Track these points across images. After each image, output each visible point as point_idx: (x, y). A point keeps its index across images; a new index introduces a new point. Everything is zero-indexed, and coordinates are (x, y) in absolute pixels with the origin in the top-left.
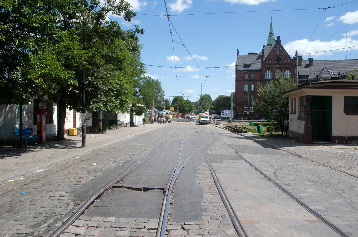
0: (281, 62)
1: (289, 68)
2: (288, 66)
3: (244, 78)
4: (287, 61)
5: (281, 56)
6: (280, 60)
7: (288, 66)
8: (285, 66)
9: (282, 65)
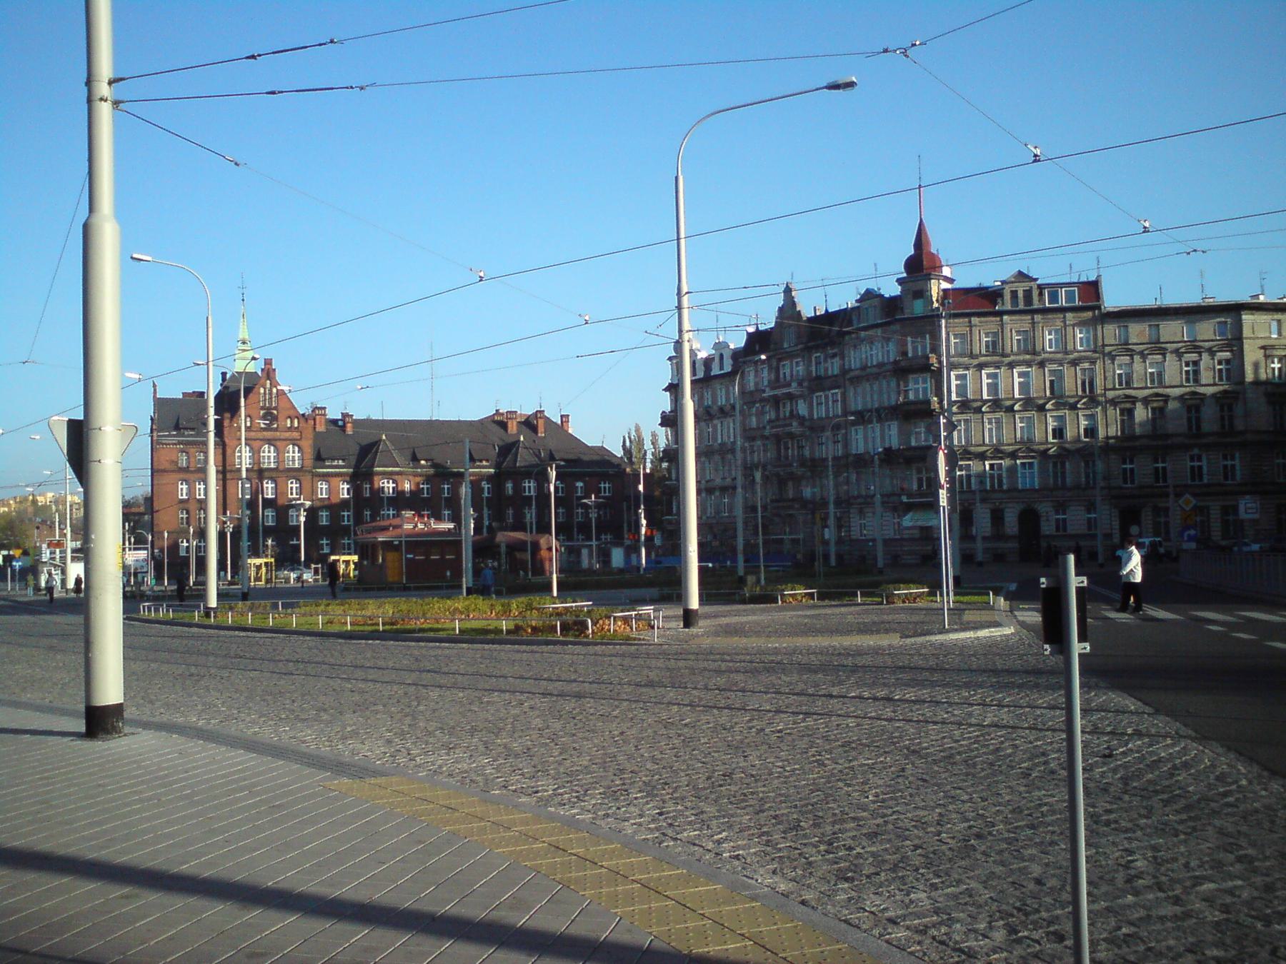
0: (275, 426)
1: (295, 440)
2: (296, 435)
3: (177, 463)
4: (292, 422)
5: (275, 408)
6: (275, 418)
7: (296, 435)
8: (287, 435)
9: (278, 433)
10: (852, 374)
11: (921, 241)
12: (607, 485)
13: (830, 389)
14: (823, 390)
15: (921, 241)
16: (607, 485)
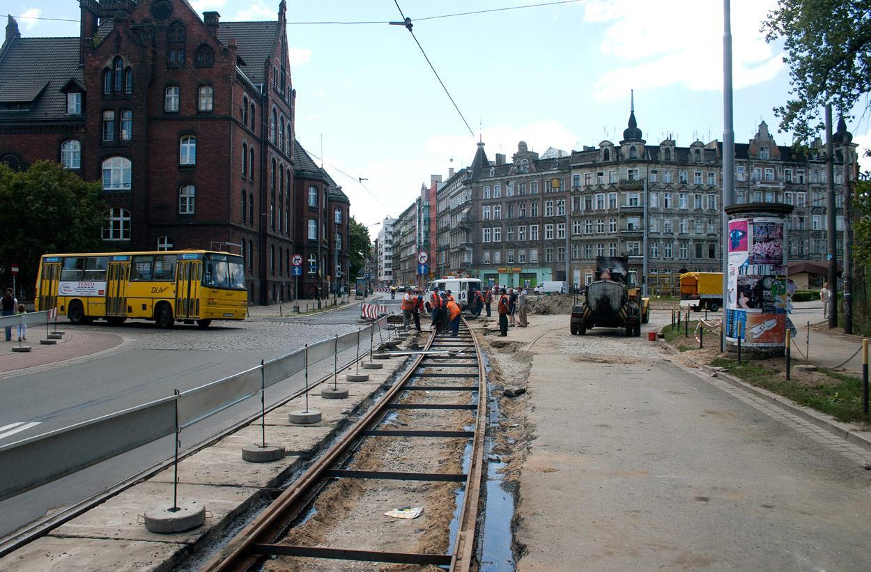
10: (814, 185)
11: (632, 121)
12: (122, 219)
13: (797, 191)
14: (793, 191)
15: (632, 121)
16: (122, 219)
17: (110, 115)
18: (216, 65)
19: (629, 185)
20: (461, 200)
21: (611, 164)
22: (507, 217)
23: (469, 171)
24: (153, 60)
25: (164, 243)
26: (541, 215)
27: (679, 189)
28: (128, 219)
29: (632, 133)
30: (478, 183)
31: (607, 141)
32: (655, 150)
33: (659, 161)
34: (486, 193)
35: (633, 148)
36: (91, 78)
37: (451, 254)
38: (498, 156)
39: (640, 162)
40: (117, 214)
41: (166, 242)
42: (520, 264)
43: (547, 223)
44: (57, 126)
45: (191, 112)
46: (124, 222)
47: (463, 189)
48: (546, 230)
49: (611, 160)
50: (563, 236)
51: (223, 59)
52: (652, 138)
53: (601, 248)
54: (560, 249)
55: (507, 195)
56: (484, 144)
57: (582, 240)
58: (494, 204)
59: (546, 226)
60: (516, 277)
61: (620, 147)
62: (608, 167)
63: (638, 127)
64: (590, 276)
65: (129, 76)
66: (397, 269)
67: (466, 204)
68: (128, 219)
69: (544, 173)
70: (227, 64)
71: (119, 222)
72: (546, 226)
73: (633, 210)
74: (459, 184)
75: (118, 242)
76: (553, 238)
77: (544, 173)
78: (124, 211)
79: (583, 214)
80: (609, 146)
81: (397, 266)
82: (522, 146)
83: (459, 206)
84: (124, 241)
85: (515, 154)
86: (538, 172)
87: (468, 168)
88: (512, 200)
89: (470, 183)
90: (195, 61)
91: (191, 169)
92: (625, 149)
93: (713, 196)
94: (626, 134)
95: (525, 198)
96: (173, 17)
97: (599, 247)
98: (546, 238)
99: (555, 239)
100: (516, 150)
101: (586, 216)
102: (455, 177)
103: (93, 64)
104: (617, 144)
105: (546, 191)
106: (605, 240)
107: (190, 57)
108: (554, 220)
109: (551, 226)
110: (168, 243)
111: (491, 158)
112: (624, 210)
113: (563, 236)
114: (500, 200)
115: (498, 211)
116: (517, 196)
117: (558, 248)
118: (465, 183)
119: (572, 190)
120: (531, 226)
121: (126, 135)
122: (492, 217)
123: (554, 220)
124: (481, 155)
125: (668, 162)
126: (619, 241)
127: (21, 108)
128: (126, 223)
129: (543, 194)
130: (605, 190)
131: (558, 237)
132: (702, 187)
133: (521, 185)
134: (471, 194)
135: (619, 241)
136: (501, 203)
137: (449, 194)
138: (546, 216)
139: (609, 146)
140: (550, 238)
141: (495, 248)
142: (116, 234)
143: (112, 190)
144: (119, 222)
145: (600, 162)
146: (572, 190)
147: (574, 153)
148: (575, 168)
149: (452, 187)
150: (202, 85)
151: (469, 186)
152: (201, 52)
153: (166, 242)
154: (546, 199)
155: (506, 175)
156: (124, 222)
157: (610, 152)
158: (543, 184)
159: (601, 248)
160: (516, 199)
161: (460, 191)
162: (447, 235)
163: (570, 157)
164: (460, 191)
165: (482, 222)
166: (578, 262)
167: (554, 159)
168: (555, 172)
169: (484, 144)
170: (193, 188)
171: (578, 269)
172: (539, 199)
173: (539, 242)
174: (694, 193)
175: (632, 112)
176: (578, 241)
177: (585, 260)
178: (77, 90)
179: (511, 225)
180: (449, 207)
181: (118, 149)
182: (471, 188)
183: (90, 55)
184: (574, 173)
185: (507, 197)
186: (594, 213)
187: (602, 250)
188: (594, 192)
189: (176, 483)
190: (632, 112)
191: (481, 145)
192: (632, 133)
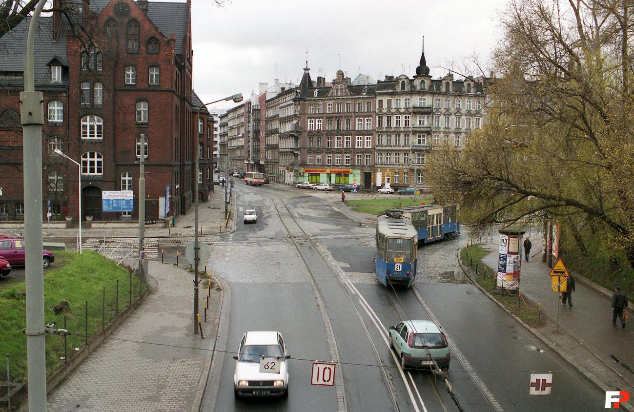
11: (423, 61)
12: (96, 159)
15: (423, 61)
16: (96, 159)
17: (86, 87)
18: (162, 52)
19: (419, 111)
20: (290, 112)
21: (407, 93)
22: (327, 129)
23: (298, 91)
24: (117, 47)
25: (126, 177)
26: (353, 129)
27: (455, 114)
28: (131, 178)
29: (422, 70)
30: (305, 101)
31: (403, 75)
32: (439, 82)
33: (441, 92)
34: (311, 110)
35: (423, 82)
36: (72, 58)
37: (280, 152)
38: (319, 78)
39: (427, 93)
40: (92, 156)
41: (127, 176)
42: (336, 165)
43: (357, 135)
44: (53, 91)
45: (144, 86)
46: (98, 162)
47: (292, 104)
48: (357, 140)
49: (406, 90)
50: (370, 146)
51: (166, 49)
52: (436, 74)
53: (397, 156)
54: (367, 156)
55: (327, 112)
56: (309, 70)
57: (383, 150)
58: (317, 118)
59: (357, 137)
60: (333, 176)
61: (413, 80)
62: (404, 96)
63: (427, 65)
64: (389, 177)
65: (99, 58)
66: (224, 155)
67: (295, 116)
68: (131, 178)
69: (356, 97)
70: (169, 52)
71: (94, 162)
72: (357, 137)
73: (422, 129)
74: (289, 98)
75: (93, 176)
76: (362, 147)
77: (356, 97)
78: (97, 154)
79: (384, 130)
80: (405, 79)
81: (224, 152)
82: (340, 74)
83: (288, 116)
84: (98, 175)
85: (334, 80)
86: (351, 95)
87: (297, 88)
88: (330, 115)
89: (299, 101)
90: (147, 49)
91: (145, 126)
92: (417, 83)
93: (479, 119)
94: (418, 70)
95: (341, 115)
96: (130, 16)
97: (396, 155)
98: (356, 147)
99: (363, 148)
100: (335, 77)
101: (386, 132)
102: (284, 93)
103: (73, 48)
104: (411, 78)
105: (357, 111)
106: (401, 150)
107: (142, 46)
108: (362, 133)
109: (361, 138)
110: (128, 177)
111: (314, 78)
112: (415, 129)
113: (370, 146)
114: (321, 116)
115: (319, 123)
116: (335, 113)
117: (365, 155)
118: (294, 100)
119: (377, 111)
120: (345, 137)
121: (99, 101)
122: (315, 128)
123: (362, 133)
124: (307, 78)
125: (447, 94)
126: (411, 152)
127: (16, 76)
128: (99, 163)
129: (355, 113)
130: (402, 113)
131: (365, 147)
132: (471, 112)
133: (338, 104)
134: (299, 109)
135: (411, 152)
136: (322, 118)
137: (279, 105)
138: (357, 129)
139: (405, 79)
140: (359, 147)
141: (317, 153)
142: (92, 170)
143: (88, 139)
144: (94, 162)
145: (399, 91)
146: (377, 111)
147: (379, 82)
148: (380, 94)
149: (281, 100)
150: (153, 66)
151: (297, 103)
152: (150, 43)
153: (127, 176)
154: (357, 117)
155: (327, 96)
156: (98, 162)
157: (406, 84)
158: (355, 105)
159: (397, 156)
160: (334, 115)
161: (290, 105)
162: (276, 136)
163: (376, 85)
164: (290, 105)
165: (307, 131)
166: (380, 166)
167: (364, 86)
168: (365, 97)
169: (309, 70)
170: (141, 134)
171: (381, 171)
172: (352, 116)
173: (351, 150)
174: (466, 116)
175: (423, 53)
176: (381, 150)
177: (385, 165)
178: (58, 64)
179: (330, 135)
180: (278, 115)
181: (92, 111)
182: (299, 104)
183: (71, 41)
184: (379, 98)
185: (327, 113)
186: (393, 130)
187: (398, 158)
188: (393, 114)
189: (214, 351)
190: (423, 53)
191: (306, 69)
192: (422, 70)
